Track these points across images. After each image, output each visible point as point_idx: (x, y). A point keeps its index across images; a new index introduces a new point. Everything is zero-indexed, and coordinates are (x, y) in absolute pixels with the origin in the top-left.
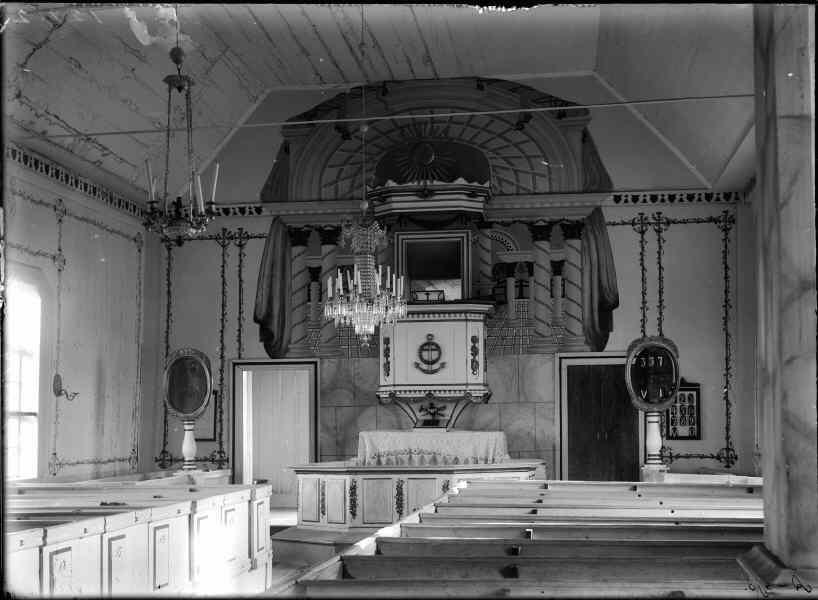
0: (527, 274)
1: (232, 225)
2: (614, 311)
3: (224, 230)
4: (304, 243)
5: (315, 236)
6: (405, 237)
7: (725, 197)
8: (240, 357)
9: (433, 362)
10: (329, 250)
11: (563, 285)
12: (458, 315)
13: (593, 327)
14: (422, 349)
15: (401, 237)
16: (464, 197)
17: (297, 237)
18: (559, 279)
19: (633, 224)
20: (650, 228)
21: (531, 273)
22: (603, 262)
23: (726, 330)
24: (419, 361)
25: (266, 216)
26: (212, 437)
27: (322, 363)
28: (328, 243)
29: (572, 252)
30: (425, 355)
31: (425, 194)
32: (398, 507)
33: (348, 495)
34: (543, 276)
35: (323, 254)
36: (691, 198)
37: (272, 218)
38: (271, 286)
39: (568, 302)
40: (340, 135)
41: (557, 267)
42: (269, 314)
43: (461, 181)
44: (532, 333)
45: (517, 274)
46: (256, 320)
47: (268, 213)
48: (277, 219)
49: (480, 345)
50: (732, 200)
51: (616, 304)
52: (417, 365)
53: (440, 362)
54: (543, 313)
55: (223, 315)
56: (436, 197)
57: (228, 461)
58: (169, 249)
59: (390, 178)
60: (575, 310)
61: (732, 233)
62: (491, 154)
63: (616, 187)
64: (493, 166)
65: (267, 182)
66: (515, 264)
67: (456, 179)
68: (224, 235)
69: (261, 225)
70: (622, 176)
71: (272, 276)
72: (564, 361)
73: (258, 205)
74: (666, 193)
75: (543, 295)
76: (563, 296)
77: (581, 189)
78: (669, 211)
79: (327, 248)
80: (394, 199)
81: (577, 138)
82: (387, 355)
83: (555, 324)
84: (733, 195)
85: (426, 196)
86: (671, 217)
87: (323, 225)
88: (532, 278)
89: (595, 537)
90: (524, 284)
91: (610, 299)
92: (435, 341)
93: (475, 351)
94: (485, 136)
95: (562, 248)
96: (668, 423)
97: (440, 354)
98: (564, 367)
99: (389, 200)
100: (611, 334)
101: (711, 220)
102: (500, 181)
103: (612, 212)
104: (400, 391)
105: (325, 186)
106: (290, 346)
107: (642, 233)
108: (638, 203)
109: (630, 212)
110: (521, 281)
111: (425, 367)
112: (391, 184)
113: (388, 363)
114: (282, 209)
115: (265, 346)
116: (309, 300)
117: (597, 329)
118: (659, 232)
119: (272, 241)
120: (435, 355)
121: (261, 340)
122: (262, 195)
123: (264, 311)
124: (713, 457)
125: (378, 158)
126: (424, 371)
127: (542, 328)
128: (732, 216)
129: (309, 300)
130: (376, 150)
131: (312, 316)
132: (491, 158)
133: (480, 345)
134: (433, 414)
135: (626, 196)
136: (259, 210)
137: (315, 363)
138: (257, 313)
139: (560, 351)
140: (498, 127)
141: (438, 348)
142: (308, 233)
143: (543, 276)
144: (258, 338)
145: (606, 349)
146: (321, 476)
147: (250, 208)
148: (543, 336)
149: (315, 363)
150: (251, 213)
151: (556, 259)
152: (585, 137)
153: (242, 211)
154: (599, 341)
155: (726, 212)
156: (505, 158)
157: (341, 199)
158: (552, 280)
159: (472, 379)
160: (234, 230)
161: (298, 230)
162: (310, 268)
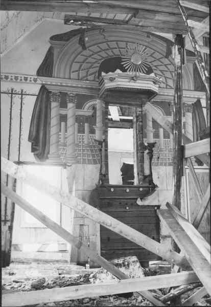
31: (133, 79)
59: (119, 68)
73: (36, 77)
112: (118, 71)
131: (62, 141)
132: (155, 70)
136: (35, 80)
156: (161, 71)
157: (81, 80)
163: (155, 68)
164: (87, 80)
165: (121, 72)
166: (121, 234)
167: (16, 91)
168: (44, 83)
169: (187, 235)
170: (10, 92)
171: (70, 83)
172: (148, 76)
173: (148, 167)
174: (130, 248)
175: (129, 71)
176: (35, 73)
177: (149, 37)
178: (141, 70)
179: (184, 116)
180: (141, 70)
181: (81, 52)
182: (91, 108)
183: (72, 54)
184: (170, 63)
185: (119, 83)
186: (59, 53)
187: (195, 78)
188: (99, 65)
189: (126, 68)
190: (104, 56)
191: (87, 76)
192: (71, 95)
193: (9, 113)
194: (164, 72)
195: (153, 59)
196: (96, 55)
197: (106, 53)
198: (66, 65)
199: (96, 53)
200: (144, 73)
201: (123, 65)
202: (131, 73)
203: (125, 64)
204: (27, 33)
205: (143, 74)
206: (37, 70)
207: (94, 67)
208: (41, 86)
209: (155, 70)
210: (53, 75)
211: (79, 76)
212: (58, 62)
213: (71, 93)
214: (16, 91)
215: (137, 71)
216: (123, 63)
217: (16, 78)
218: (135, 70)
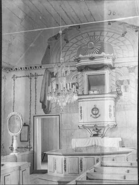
14: (93, 110)
21: (129, 84)
31: (92, 59)
46: (41, 102)
53: (99, 114)
57: (32, 148)
58: (14, 80)
62: (113, 45)
68: (30, 75)
73: (41, 65)
88: (129, 85)
90: (127, 87)
99: (80, 61)
110: (126, 86)
111: (94, 116)
115: (44, 110)
119: (45, 76)
122: (42, 62)
136: (41, 67)
156: (119, 46)
165: (82, 56)
167: (32, 74)
174: (127, 61)
177: (110, 24)
178: (95, 52)
179: (82, 151)
180: (95, 52)
181: (66, 44)
184: (113, 34)
185: (81, 63)
188: (77, 51)
193: (35, 87)
196: (75, 45)
200: (97, 53)
203: (97, 51)
204: (25, 31)
205: (97, 54)
208: (45, 69)
214: (32, 74)
215: (92, 53)
217: (36, 67)
218: (92, 53)
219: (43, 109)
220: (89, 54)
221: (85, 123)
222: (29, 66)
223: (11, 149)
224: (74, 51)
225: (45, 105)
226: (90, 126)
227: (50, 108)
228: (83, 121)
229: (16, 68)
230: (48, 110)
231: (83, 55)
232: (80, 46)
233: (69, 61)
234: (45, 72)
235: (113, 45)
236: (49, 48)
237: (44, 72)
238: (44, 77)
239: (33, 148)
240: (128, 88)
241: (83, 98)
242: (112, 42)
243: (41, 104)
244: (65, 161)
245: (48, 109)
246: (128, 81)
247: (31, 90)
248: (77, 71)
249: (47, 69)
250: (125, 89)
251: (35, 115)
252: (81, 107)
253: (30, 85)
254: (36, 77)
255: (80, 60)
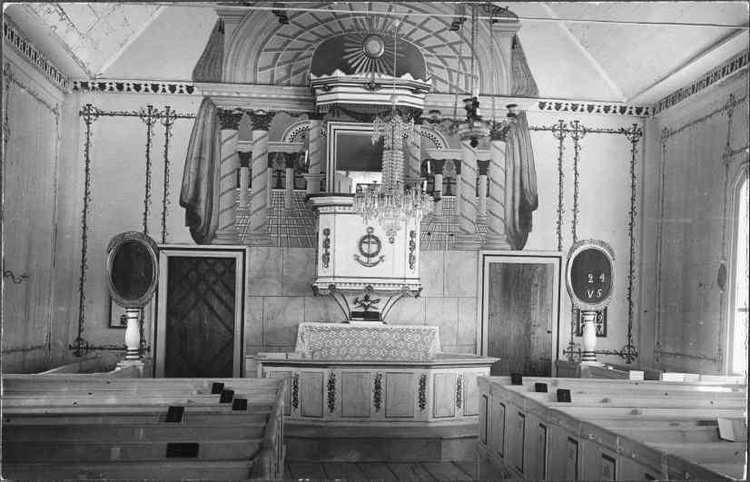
0: (455, 172)
1: (159, 102)
2: (534, 213)
3: (150, 107)
4: (235, 127)
5: (246, 121)
6: (336, 127)
7: (572, 108)
8: (164, 242)
9: (373, 255)
10: (228, 136)
11: (488, 185)
12: (347, 208)
13: (514, 226)
14: (362, 242)
15: (333, 127)
16: (410, 93)
17: (228, 119)
18: (484, 178)
19: (553, 130)
20: (568, 135)
21: (459, 172)
22: (525, 164)
23: (631, 235)
24: (359, 254)
25: (197, 96)
26: (112, 325)
27: (250, 251)
28: (230, 127)
29: (497, 153)
30: (365, 247)
31: (372, 87)
32: (375, 401)
33: (326, 389)
34: (469, 173)
35: (254, 139)
36: (607, 109)
37: (202, 98)
38: (198, 169)
39: (492, 201)
40: (278, 18)
41: (483, 167)
42: (196, 198)
43: (407, 77)
44: (458, 230)
45: (445, 171)
46: (182, 204)
47: (201, 93)
48: (207, 100)
49: (417, 241)
50: (642, 114)
51: (535, 206)
52: (358, 259)
53: (380, 254)
54: (469, 210)
55: (147, 197)
56: (382, 91)
57: (149, 349)
58: (88, 124)
59: (338, 68)
60: (499, 210)
61: (639, 146)
62: (425, 52)
63: (541, 95)
64: (428, 63)
65: (199, 61)
66: (444, 160)
67: (404, 74)
68: (149, 112)
69: (189, 105)
70: (546, 88)
71: (200, 158)
72: (241, 254)
73: (190, 84)
74: (603, 104)
75: (469, 193)
76: (488, 196)
77: (510, 94)
78: (587, 120)
79: (258, 133)
80: (340, 89)
81: (507, 44)
82: (326, 245)
83: (479, 222)
84: (644, 110)
85: (373, 89)
86: (101, 107)
87: (255, 109)
88: (459, 177)
89: (113, 421)
90: (452, 181)
91: (530, 201)
92: (375, 234)
93: (412, 247)
94: (421, 33)
95: (488, 149)
96: (578, 321)
97: (379, 247)
98: (487, 265)
99: (334, 90)
100: (530, 234)
101: (622, 131)
102: (435, 78)
103: (535, 116)
104: (341, 283)
105: (261, 70)
106: (217, 232)
107: (561, 139)
108: (141, 91)
109: (551, 118)
110: (449, 179)
111: (364, 259)
112: (338, 73)
113: (328, 254)
114: (212, 90)
115: (192, 231)
116: (239, 186)
117: (518, 229)
118: (576, 139)
119: (201, 121)
120: (374, 248)
121: (187, 225)
122: (195, 73)
123: (191, 192)
124: (617, 354)
125: (315, 46)
126: (363, 264)
127: (469, 227)
128: (639, 130)
129: (239, 186)
130: (314, 38)
131: (242, 203)
132: (427, 56)
133: (417, 241)
134: (366, 307)
135: (551, 103)
136: (190, 90)
137: (244, 251)
138: (184, 196)
139: (483, 248)
140: (435, 26)
141: (378, 241)
142: (239, 117)
143: (469, 173)
144: (184, 224)
145: (525, 248)
146: (293, 370)
147: (615, 107)
148: (468, 233)
149: (244, 251)
150: (164, 91)
151: (244, 151)
152: (515, 42)
153: (173, 89)
154: (519, 241)
155: (635, 125)
156: (441, 58)
157: (277, 84)
158: (478, 179)
159: (409, 274)
160: (161, 109)
161: (228, 113)
162: (240, 153)
163: (429, 53)
164: (288, 85)
166: (532, 286)
168: (206, 93)
169: (408, 439)
170: (147, 113)
171: (255, 92)
172: (398, 80)
173: (511, 190)
175: (360, 71)
176: (189, 76)
181: (278, 28)
182: (299, 137)
183: (261, 32)
186: (235, 33)
187: (514, 70)
188: (313, 52)
189: (353, 66)
190: (323, 34)
191: (288, 76)
192: (261, 113)
194: (447, 60)
195: (425, 34)
197: (327, 27)
198: (249, 55)
199: (307, 28)
201: (348, 59)
202: (364, 76)
203: (353, 63)
206: (192, 69)
207: (303, 58)
209: (427, 56)
210: (223, 78)
211: (272, 76)
212: (232, 53)
213: (258, 111)
214: (156, 110)
216: (345, 57)
218: (371, 70)
219: (188, 228)
220: (366, 70)
221: (337, 280)
222: (149, 83)
223: (75, 351)
224: (305, 53)
225: (196, 215)
226: (348, 287)
227: (212, 225)
228: (330, 274)
229: (102, 81)
230: (205, 231)
231: (347, 74)
232: (323, 41)
233: (285, 82)
234: (201, 107)
235: (425, 52)
236: (223, 33)
237: (199, 105)
238: (196, 124)
239: (152, 349)
240: (455, 184)
241: (335, 205)
242: (422, 42)
243: (184, 210)
244: (332, 382)
245: (207, 232)
246: (458, 163)
247: (148, 163)
248: (307, 116)
249: (206, 99)
250: (445, 186)
251: (162, 246)
252: (328, 230)
253: (148, 145)
254: (170, 122)
255: (332, 87)
